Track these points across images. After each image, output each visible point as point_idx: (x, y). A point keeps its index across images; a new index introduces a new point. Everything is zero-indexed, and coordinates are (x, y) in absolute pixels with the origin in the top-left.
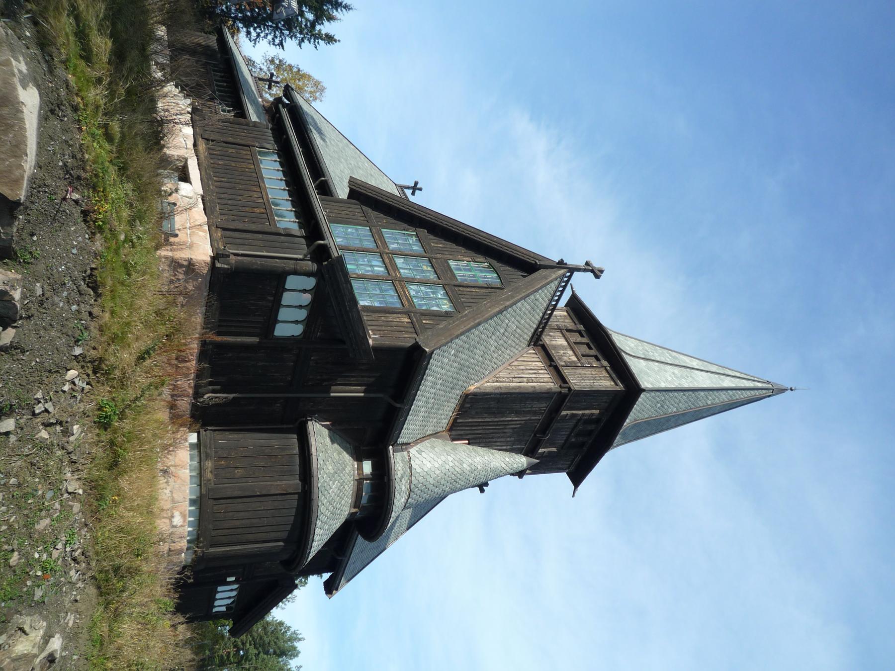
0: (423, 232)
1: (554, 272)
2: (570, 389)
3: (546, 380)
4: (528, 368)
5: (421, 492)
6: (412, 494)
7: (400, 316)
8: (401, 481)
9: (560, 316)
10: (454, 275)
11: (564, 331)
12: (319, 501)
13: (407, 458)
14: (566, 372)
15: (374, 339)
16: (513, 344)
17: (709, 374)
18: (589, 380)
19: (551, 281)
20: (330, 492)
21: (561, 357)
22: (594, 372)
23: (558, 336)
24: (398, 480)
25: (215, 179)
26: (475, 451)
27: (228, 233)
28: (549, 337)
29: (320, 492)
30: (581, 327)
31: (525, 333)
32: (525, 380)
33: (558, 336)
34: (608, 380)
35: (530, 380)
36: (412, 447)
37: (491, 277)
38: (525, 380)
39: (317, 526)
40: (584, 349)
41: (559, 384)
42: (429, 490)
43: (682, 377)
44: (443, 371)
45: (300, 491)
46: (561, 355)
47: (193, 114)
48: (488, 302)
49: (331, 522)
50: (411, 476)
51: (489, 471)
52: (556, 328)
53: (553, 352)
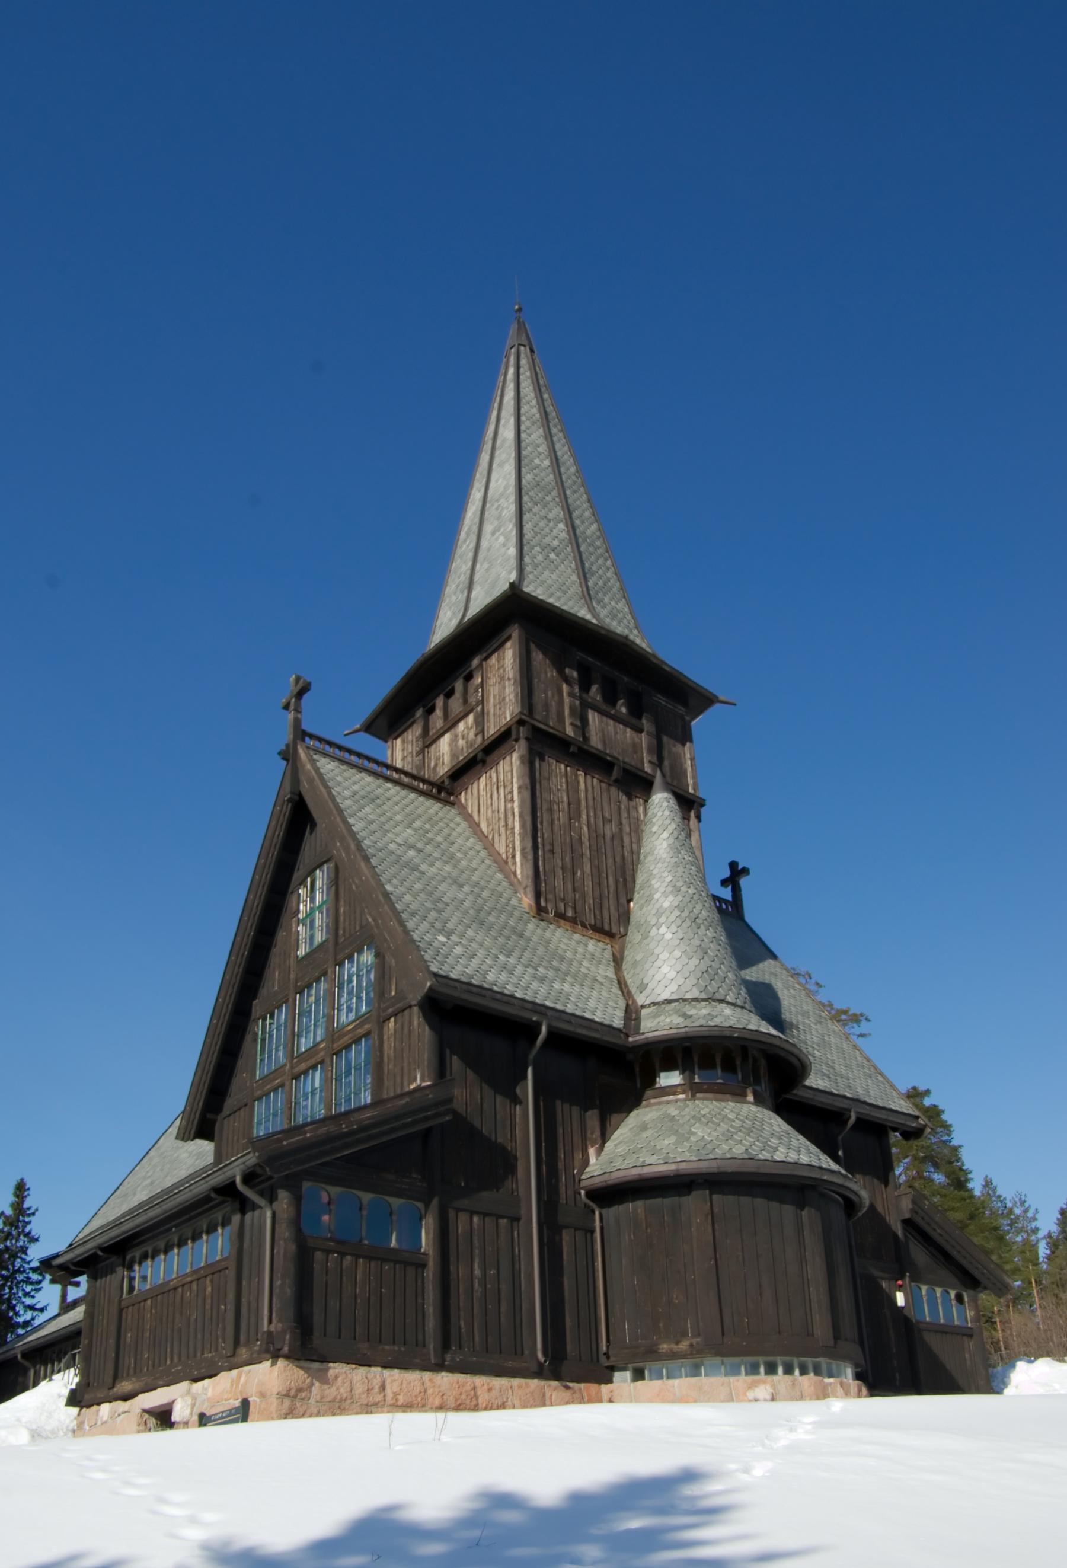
0: (257, 1007)
1: (304, 766)
2: (520, 722)
3: (507, 768)
4: (489, 803)
5: (714, 979)
6: (718, 996)
7: (385, 1037)
8: (691, 1016)
9: (403, 750)
10: (321, 945)
11: (428, 741)
12: (724, 1156)
13: (653, 1008)
14: (492, 729)
15: (423, 1080)
16: (446, 831)
17: (495, 466)
18: (504, 688)
19: (317, 770)
20: (710, 1139)
21: (469, 744)
22: (493, 680)
23: (436, 752)
24: (688, 1023)
25: (168, 1362)
26: (642, 888)
27: (243, 1338)
28: (438, 769)
29: (707, 1157)
30: (419, 713)
31: (426, 812)
32: (509, 805)
33: (436, 752)
34: (504, 653)
35: (509, 797)
36: (634, 1001)
37: (321, 878)
38: (509, 805)
39: (770, 1158)
40: (456, 704)
41: (514, 743)
42: (710, 967)
43: (499, 517)
44: (481, 953)
45: (707, 1192)
46: (467, 742)
47: (83, 1404)
48: (354, 881)
49: (766, 1134)
50: (685, 1000)
51: (677, 859)
52: (421, 757)
53: (461, 758)
